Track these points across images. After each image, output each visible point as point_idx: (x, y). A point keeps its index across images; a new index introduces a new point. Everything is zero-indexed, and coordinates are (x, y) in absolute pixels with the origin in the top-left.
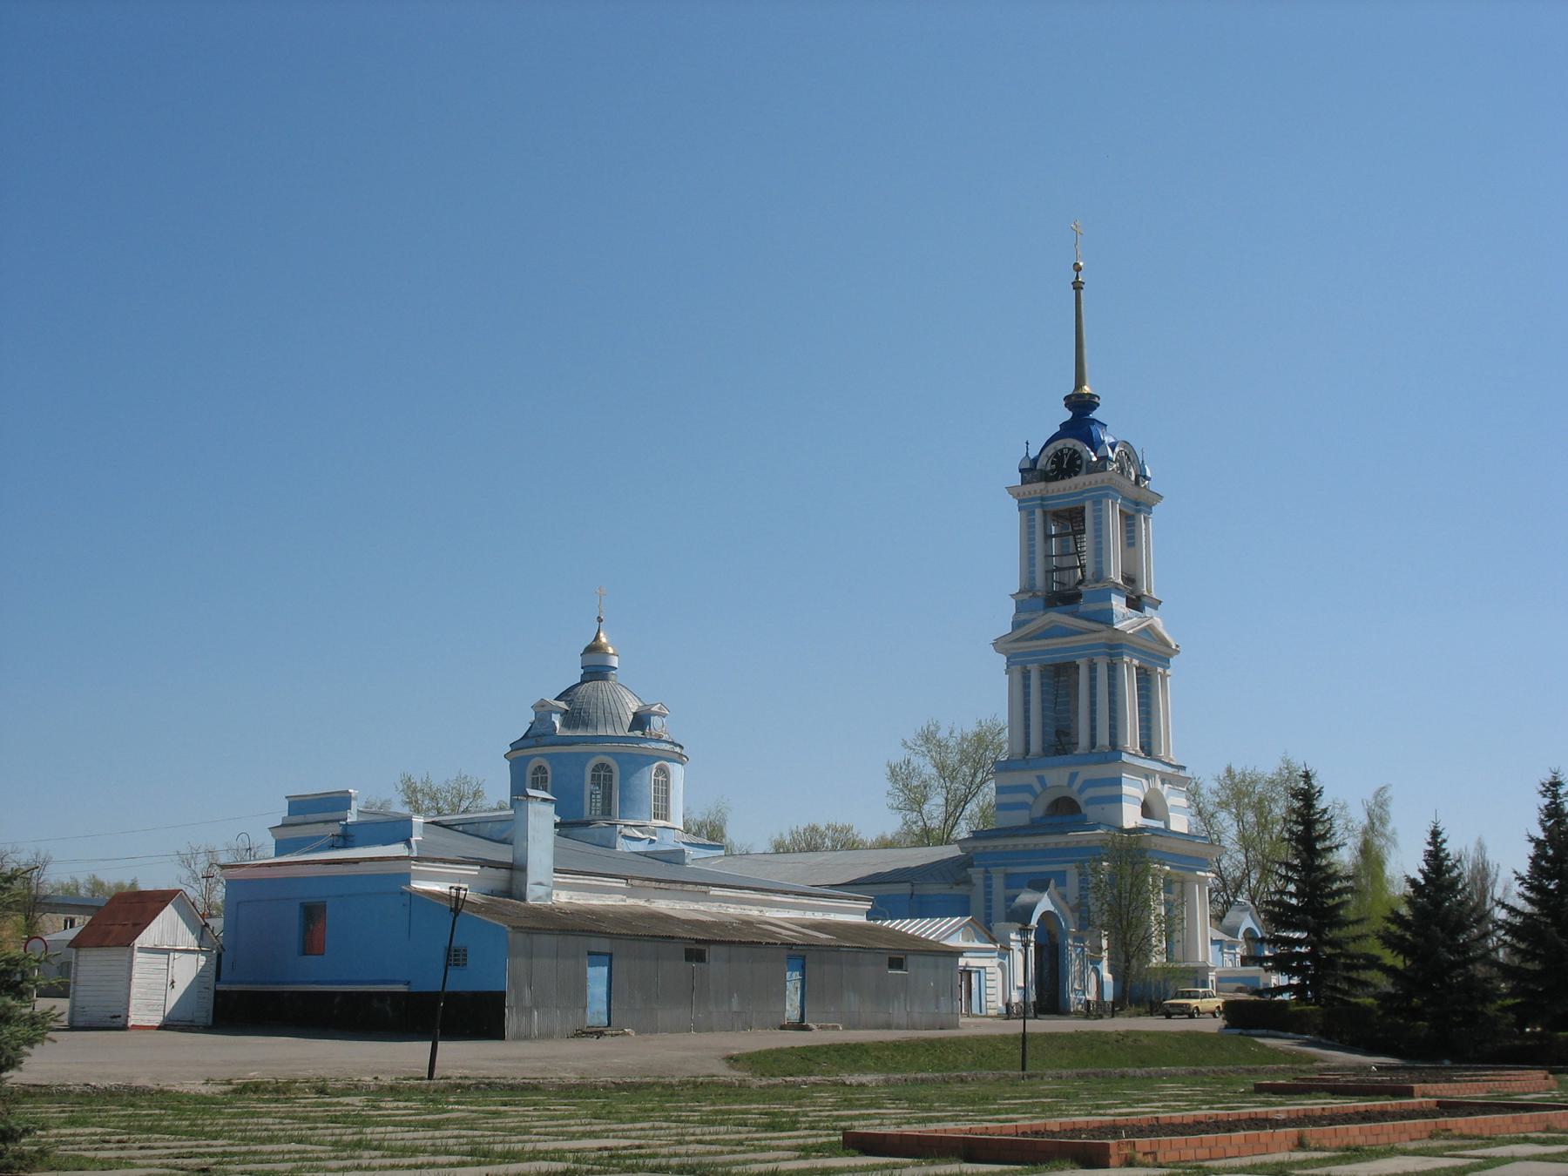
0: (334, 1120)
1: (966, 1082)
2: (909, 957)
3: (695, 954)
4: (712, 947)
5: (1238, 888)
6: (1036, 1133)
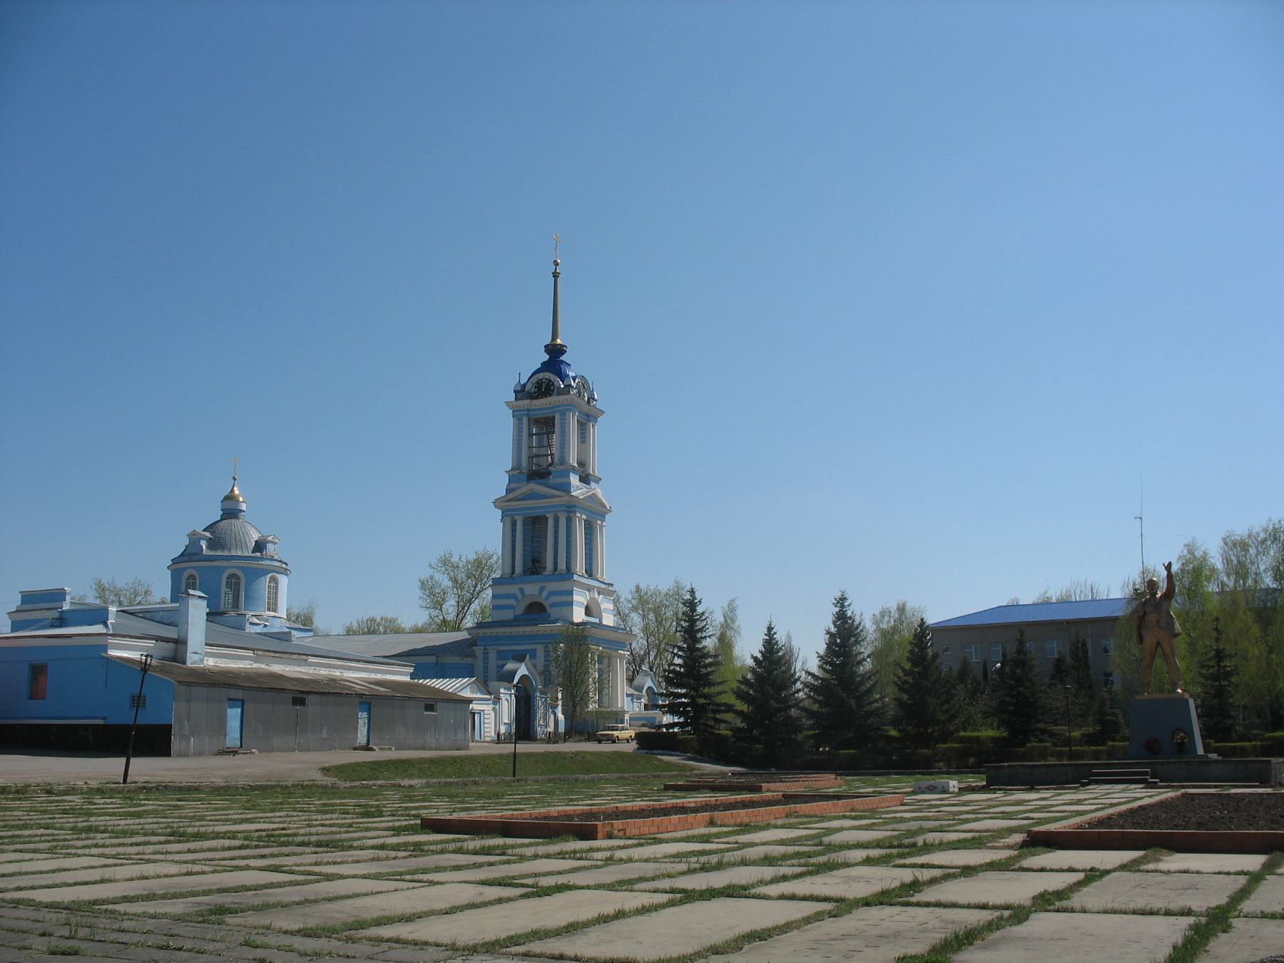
0: (65, 812)
1: (478, 785)
2: (438, 704)
3: (299, 701)
4: (310, 696)
5: (642, 661)
6: (545, 818)
